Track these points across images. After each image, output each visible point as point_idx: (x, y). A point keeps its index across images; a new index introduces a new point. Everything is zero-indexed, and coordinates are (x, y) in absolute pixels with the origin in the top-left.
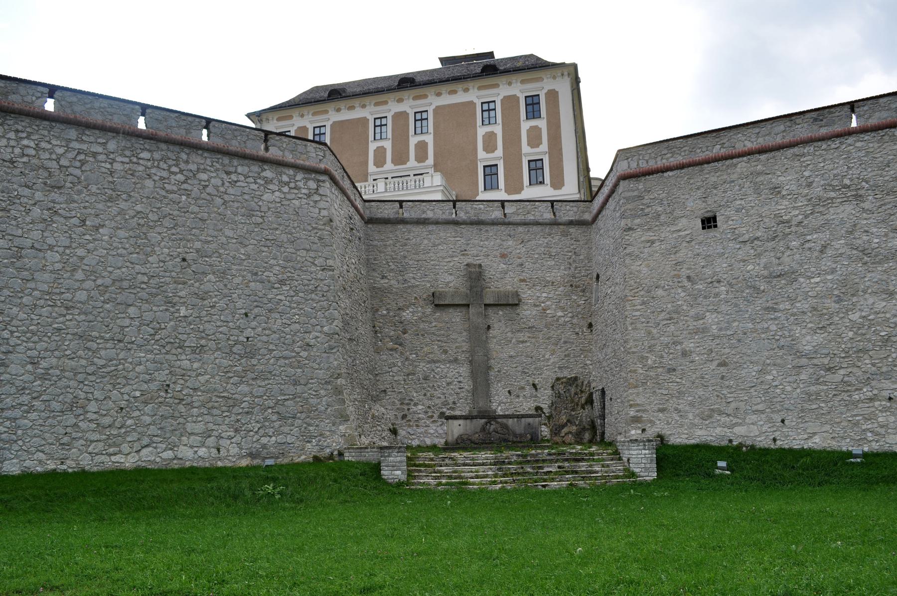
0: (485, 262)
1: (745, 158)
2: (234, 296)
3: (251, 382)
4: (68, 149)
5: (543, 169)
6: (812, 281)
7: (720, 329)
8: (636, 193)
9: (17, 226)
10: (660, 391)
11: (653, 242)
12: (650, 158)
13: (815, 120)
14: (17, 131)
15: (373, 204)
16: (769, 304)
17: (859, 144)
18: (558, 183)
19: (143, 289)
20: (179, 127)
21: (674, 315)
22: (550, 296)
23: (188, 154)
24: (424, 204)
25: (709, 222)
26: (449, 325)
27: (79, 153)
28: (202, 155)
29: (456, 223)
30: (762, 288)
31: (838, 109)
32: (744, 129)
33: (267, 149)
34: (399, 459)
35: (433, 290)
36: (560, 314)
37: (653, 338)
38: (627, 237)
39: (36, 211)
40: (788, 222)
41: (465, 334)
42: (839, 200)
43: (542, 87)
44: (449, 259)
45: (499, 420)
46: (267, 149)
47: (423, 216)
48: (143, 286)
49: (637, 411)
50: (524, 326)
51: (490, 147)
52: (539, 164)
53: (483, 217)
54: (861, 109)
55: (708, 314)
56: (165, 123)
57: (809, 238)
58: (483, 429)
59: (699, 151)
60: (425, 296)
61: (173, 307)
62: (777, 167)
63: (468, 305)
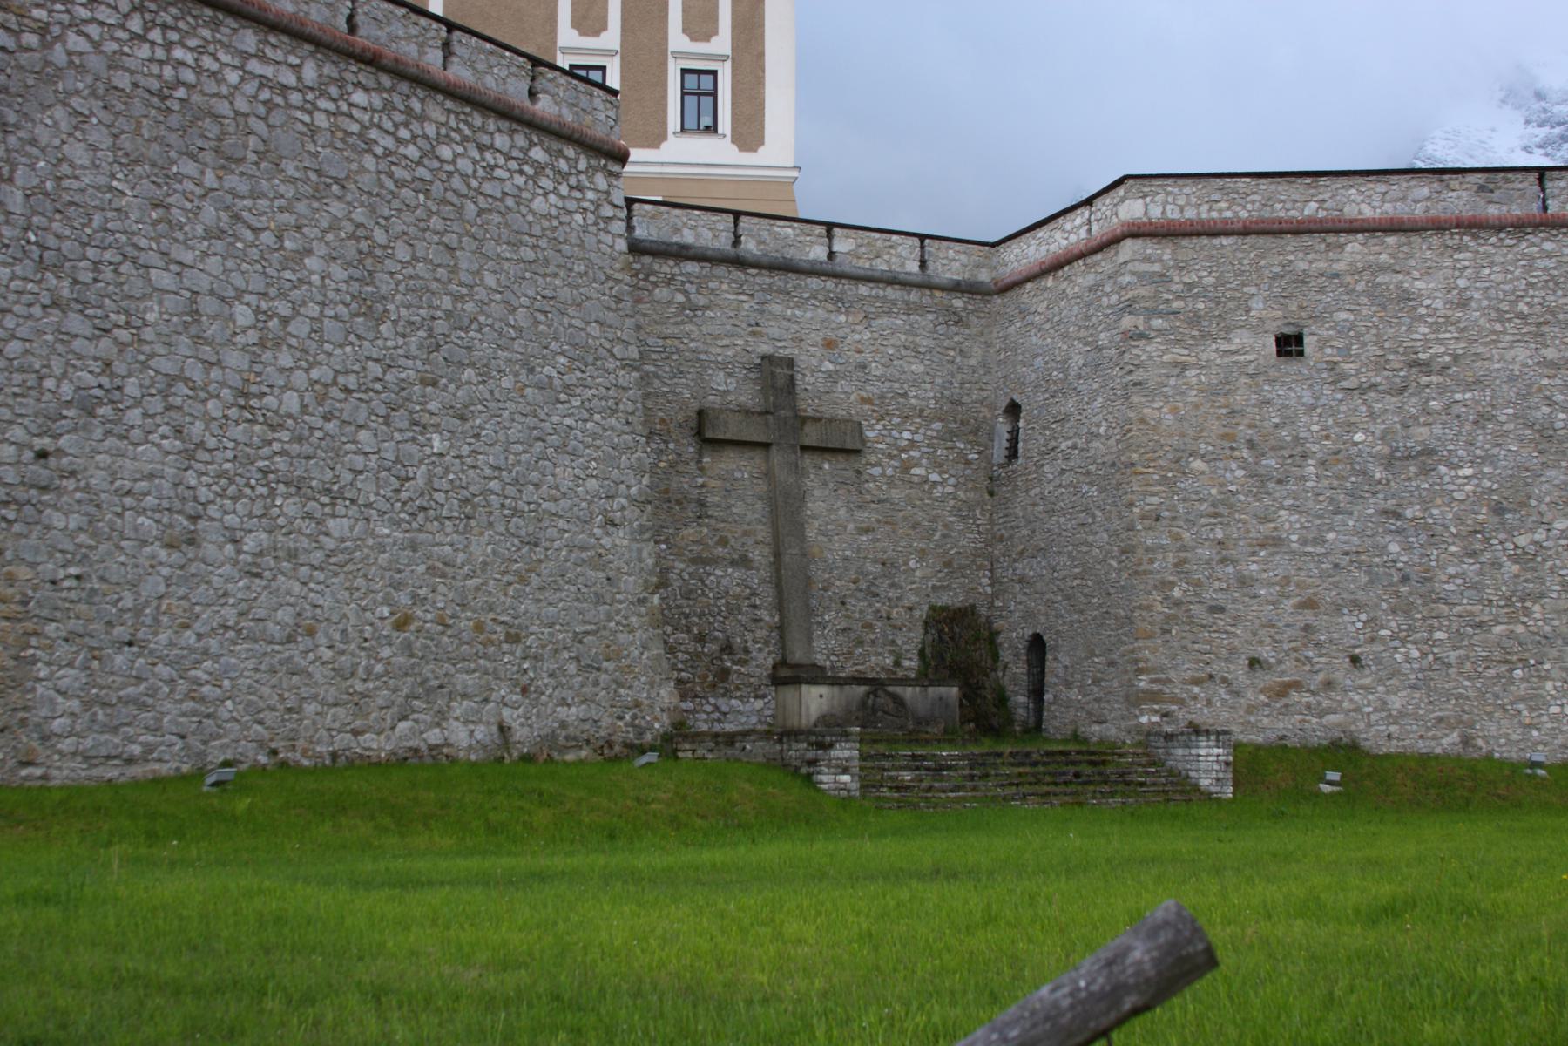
1: (1360, 236)
2: (506, 414)
3: (538, 595)
4: (247, 76)
5: (714, 95)
6: (1461, 473)
7: (1304, 542)
8: (1157, 268)
9: (185, 242)
10: (1196, 646)
11: (1184, 367)
12: (1188, 204)
13: (1482, 188)
14: (164, 27)
16: (1390, 504)
17: (1548, 246)
18: (749, 134)
19: (376, 392)
20: (409, 38)
21: (1222, 509)
23: (422, 101)
24: (677, 212)
25: (1289, 345)
27: (262, 86)
28: (442, 104)
30: (1378, 476)
31: (1519, 176)
32: (1360, 180)
33: (532, 94)
34: (847, 753)
35: (695, 405)
36: (934, 477)
37: (1184, 548)
38: (1135, 351)
39: (209, 212)
40: (1426, 364)
41: (759, 505)
42: (1508, 338)
44: (726, 342)
45: (890, 689)
46: (532, 94)
47: (675, 239)
48: (378, 386)
49: (1153, 681)
50: (869, 497)
52: (706, 82)
54: (1557, 183)
55: (1282, 513)
56: (387, 30)
57: (1458, 396)
58: (863, 704)
59: (1278, 206)
60: (680, 417)
61: (422, 434)
62: (1413, 263)
63: (766, 446)
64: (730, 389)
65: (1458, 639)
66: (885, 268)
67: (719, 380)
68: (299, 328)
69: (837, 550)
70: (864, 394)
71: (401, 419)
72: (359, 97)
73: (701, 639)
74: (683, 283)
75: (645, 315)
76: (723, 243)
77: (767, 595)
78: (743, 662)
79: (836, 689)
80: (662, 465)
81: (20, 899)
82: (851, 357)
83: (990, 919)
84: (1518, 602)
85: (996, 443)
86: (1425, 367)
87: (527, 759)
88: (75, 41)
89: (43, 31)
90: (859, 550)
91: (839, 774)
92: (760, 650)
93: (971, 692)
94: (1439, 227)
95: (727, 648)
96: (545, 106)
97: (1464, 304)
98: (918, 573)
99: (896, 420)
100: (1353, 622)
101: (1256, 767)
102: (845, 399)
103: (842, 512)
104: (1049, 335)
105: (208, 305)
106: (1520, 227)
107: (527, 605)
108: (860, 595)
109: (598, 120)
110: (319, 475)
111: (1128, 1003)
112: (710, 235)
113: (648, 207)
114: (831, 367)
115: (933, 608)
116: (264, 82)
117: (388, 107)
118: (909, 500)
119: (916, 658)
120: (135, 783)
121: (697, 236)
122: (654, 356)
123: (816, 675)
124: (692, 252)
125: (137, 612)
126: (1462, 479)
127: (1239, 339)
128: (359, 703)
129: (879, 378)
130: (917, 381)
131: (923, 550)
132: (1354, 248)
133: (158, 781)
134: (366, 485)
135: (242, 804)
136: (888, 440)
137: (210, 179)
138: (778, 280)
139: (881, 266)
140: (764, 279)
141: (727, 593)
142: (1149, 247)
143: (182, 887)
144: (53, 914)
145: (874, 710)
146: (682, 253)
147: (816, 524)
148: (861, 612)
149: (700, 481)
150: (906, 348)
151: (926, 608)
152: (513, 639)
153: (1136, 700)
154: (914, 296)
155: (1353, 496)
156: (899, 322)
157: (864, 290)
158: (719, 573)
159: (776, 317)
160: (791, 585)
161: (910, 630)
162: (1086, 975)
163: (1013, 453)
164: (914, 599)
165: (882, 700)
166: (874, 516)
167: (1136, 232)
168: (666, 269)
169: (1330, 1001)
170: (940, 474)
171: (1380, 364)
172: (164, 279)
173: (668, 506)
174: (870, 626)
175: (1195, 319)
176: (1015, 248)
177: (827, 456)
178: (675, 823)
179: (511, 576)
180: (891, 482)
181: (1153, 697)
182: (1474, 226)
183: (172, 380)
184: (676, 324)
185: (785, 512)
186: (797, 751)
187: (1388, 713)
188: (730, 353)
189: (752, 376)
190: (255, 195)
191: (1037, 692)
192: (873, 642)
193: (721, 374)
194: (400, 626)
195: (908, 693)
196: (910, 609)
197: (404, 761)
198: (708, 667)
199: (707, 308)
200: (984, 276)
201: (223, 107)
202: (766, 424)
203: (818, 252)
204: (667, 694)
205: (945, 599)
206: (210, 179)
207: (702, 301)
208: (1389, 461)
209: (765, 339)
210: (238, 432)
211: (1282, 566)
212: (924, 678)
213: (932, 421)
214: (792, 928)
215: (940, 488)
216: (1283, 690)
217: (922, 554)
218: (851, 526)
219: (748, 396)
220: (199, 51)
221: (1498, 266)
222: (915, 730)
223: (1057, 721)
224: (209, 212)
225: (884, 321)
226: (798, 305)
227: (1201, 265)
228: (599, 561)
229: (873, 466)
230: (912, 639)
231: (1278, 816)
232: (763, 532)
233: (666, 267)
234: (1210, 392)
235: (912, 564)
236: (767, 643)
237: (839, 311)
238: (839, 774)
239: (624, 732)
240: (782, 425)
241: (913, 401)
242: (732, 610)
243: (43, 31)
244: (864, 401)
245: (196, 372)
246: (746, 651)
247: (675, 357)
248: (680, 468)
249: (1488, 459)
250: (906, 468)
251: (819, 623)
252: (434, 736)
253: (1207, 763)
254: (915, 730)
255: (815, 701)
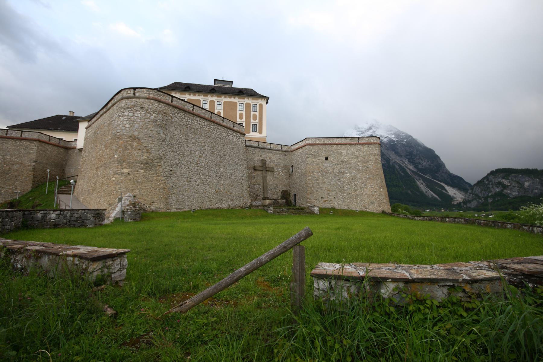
18: (260, 132)
25: (326, 159)
33: (172, 102)
39: (193, 140)
43: (259, 102)
46: (172, 102)
51: (241, 117)
64: (258, 163)
65: (347, 195)
67: (256, 162)
68: (204, 155)
69: (271, 183)
71: (217, 166)
72: (212, 127)
76: (257, 145)
77: (262, 189)
81: (166, 227)
82: (273, 160)
83: (288, 229)
84: (355, 191)
85: (291, 170)
86: (343, 161)
87: (232, 209)
88: (176, 119)
89: (171, 117)
91: (270, 211)
93: (287, 201)
94: (345, 144)
95: (257, 195)
96: (235, 128)
97: (348, 154)
100: (334, 193)
101: (321, 210)
104: (297, 157)
105: (193, 152)
106: (356, 144)
107: (232, 190)
109: (242, 130)
110: (207, 173)
111: (302, 239)
116: (200, 124)
117: (216, 128)
120: (182, 212)
123: (268, 199)
125: (183, 190)
126: (348, 175)
127: (320, 158)
128: (211, 202)
132: (335, 147)
133: (185, 211)
134: (212, 175)
135: (196, 214)
137: (193, 136)
138: (264, 150)
142: (309, 147)
143: (187, 225)
144: (170, 228)
146: (252, 147)
152: (231, 194)
153: (307, 202)
155: (334, 177)
160: (265, 187)
162: (296, 235)
163: (292, 172)
167: (308, 145)
169: (330, 240)
171: (338, 161)
172: (187, 149)
173: (250, 178)
175: (315, 155)
176: (293, 146)
178: (250, 216)
179: (230, 186)
181: (309, 202)
182: (350, 144)
183: (188, 161)
185: (264, 179)
186: (265, 208)
187: (339, 204)
190: (199, 138)
191: (295, 201)
194: (216, 192)
195: (279, 201)
197: (216, 209)
198: (255, 198)
200: (289, 150)
201: (195, 127)
203: (269, 147)
204: (250, 201)
205: (284, 189)
206: (193, 136)
208: (339, 173)
210: (196, 168)
211: (325, 186)
212: (281, 199)
214: (264, 230)
216: (325, 201)
219: (260, 164)
220: (192, 120)
221: (353, 149)
222: (280, 205)
223: (298, 204)
224: (193, 140)
227: (316, 149)
228: (241, 184)
230: (280, 194)
231: (325, 217)
232: (262, 181)
233: (250, 148)
234: (317, 164)
238: (270, 211)
239: (244, 205)
240: (265, 168)
243: (171, 117)
245: (191, 160)
249: (351, 173)
252: (221, 206)
253: (316, 210)
254: (280, 205)
255: (268, 202)
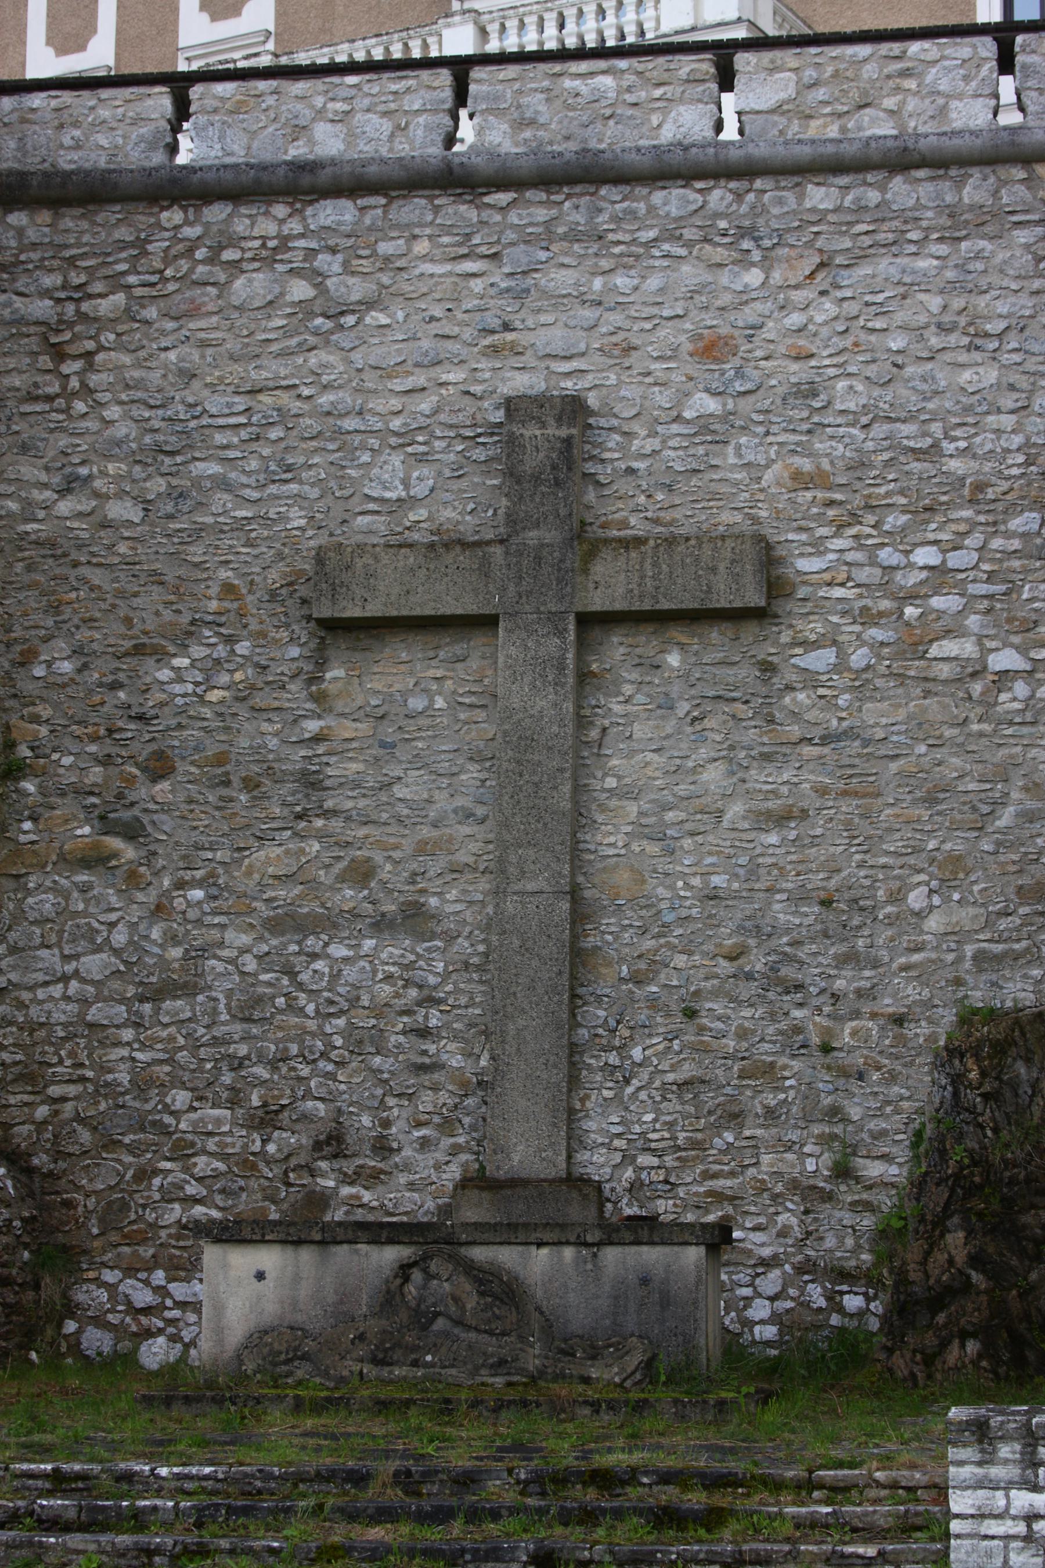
0: (593, 381)
15: (37, 100)
22: (955, 560)
24: (300, 87)
26: (388, 732)
29: (455, 181)
35: (314, 541)
36: (1006, 659)
41: (472, 774)
44: (420, 379)
45: (479, 1254)
47: (296, 151)
50: (795, 731)
53: (614, 139)
58: (389, 1299)
60: (274, 576)
63: (487, 622)
66: (887, 129)
67: (388, 476)
70: (806, 465)
73: (266, 1120)
74: (311, 253)
75: (204, 344)
76: (420, 143)
78: (373, 1178)
79: (307, 1255)
80: (214, 696)
90: (753, 871)
92: (425, 1144)
95: (332, 1143)
98: (933, 923)
99: (894, 521)
102: (753, 480)
103: (713, 776)
108: (747, 990)
112: (386, 126)
113: (223, 89)
114: (713, 405)
115: (967, 1018)
118: (920, 727)
119: (902, 1154)
121: (351, 137)
122: (220, 438)
124: (324, 177)
129: (852, 418)
130: (975, 408)
131: (955, 861)
136: (862, 575)
138: (573, 210)
139: (876, 127)
140: (535, 211)
141: (354, 1002)
145: (423, 1318)
146: (303, 184)
147: (632, 809)
148: (742, 1034)
149: (312, 726)
150: (944, 329)
151: (948, 1017)
154: (975, 189)
156: (922, 264)
157: (819, 196)
158: (339, 951)
159: (558, 301)
160: (561, 969)
161: (892, 1078)
164: (913, 992)
165: (445, 1284)
166: (810, 778)
168: (268, 227)
170: (1022, 650)
174: (767, 1073)
177: (676, 633)
180: (862, 685)
184: (285, 354)
185: (547, 795)
188: (425, 405)
189: (479, 454)
192: (771, 1113)
193: (396, 460)
196: (899, 1020)
199: (370, 304)
202: (485, 570)
207: (357, 289)
209: (529, 359)
213: (1013, 509)
215: (1021, 689)
217: (951, 872)
218: (736, 809)
225: (885, 266)
226: (622, 265)
229: (809, 646)
233: (266, 223)
235: (916, 899)
236: (448, 1126)
237: (744, 261)
241: (955, 465)
242: (359, 1043)
244: (801, 480)
246: (383, 1147)
247: (274, 434)
248: (258, 701)
250: (915, 644)
251: (610, 1069)
